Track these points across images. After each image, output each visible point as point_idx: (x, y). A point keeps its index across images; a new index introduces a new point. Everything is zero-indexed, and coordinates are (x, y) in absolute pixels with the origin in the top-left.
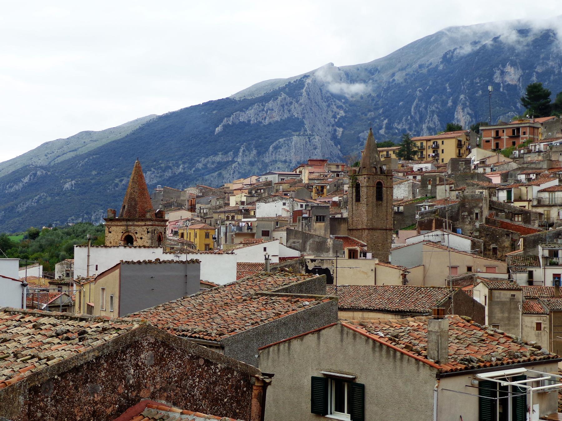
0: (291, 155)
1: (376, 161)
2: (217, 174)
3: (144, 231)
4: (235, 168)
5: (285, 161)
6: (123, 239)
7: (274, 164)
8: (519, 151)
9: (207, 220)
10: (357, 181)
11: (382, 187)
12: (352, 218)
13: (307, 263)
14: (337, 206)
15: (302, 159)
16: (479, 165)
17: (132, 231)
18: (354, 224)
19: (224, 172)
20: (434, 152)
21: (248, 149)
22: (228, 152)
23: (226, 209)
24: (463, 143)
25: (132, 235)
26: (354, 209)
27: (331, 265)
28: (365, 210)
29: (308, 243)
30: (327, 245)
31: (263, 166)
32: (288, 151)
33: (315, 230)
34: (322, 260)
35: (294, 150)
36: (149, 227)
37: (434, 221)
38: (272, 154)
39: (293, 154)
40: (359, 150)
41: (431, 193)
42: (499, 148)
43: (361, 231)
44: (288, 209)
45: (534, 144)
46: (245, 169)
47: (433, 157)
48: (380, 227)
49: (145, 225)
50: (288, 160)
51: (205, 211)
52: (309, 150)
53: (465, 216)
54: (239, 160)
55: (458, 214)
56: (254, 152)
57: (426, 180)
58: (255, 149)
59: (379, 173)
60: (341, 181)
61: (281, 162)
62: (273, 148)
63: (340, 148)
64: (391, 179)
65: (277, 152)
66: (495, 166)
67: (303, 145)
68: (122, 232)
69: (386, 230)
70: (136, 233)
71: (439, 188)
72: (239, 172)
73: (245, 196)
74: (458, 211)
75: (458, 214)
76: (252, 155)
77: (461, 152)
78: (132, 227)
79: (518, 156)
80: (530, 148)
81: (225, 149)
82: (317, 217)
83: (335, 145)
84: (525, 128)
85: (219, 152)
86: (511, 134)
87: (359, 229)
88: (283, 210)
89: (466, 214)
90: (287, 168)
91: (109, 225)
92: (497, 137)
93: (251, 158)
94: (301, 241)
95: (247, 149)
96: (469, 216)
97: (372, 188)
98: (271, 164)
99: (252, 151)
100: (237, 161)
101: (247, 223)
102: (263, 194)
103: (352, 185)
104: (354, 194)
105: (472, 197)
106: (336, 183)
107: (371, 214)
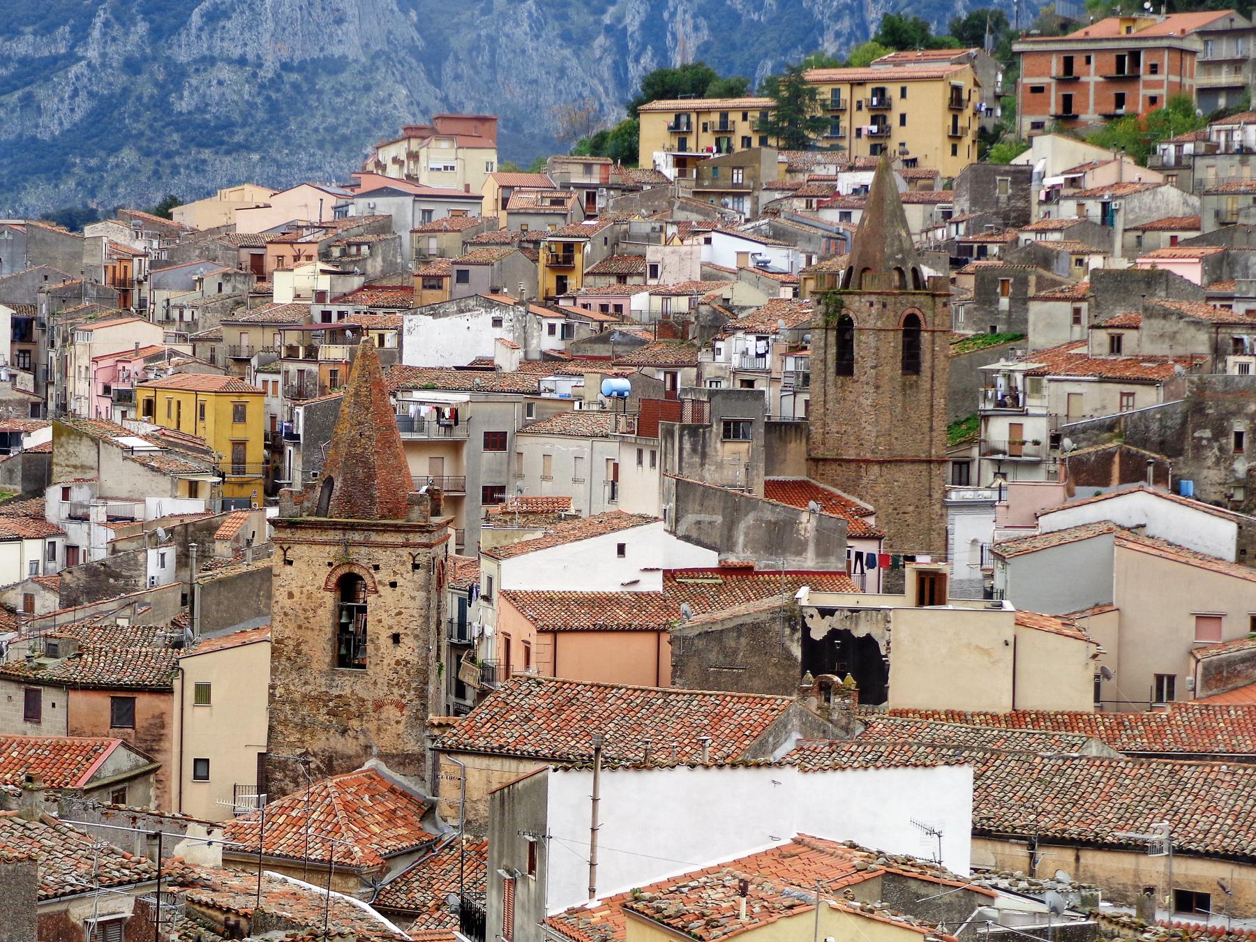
0: (263, 42)
1: (901, 250)
2: (20, 100)
3: (403, 563)
4: (77, 78)
5: (242, 61)
6: (331, 585)
7: (205, 70)
8: (1179, 146)
9: (199, 344)
10: (844, 312)
11: (919, 331)
12: (825, 425)
13: (808, 620)
14: (675, 335)
15: (298, 53)
17: (364, 562)
18: (830, 442)
19: (41, 93)
20: (874, 121)
21: (121, 17)
22: (56, 25)
23: (264, 313)
24: (965, 96)
25: (362, 572)
26: (830, 397)
28: (869, 402)
29: (742, 526)
30: (798, 530)
31: (170, 74)
32: (250, 28)
33: (720, 466)
34: (853, 611)
35: (270, 25)
36: (420, 550)
37: (1117, 459)
38: (199, 37)
39: (267, 36)
40: (477, 28)
42: (1074, 111)
43: (853, 466)
44: (509, 337)
45: (1229, 127)
46: (111, 84)
47: (871, 135)
48: (910, 454)
49: (405, 545)
50: (251, 57)
51: (187, 316)
52: (318, 25)
53: (1204, 442)
54: (93, 53)
55: (1181, 433)
56: (142, 28)
57: (995, 281)
58: (144, 19)
59: (911, 286)
60: (625, 227)
61: (230, 61)
62: (202, 16)
63: (415, 19)
64: (945, 305)
65: (215, 30)
66: (1114, 197)
67: (301, 8)
68: (330, 564)
69: (929, 462)
70: (377, 568)
71: (1035, 308)
72: (91, 95)
73: (324, 272)
74: (1184, 423)
75: (1181, 433)
76: (134, 38)
77: (960, 124)
78: (363, 550)
79: (1173, 161)
80: (1214, 138)
81: (42, 17)
83: (401, 10)
84: (1157, 55)
85: (25, 25)
86: (1112, 72)
88: (498, 344)
89: (1207, 433)
90: (247, 82)
91: (284, 541)
92: (1069, 76)
93: (129, 48)
94: (719, 519)
95: (117, 18)
96: (1217, 440)
97: (892, 333)
98: (197, 70)
99: (135, 25)
100: (83, 58)
101: (438, 410)
102: (369, 261)
103: (827, 322)
104: (833, 350)
105: (1226, 385)
106: (608, 234)
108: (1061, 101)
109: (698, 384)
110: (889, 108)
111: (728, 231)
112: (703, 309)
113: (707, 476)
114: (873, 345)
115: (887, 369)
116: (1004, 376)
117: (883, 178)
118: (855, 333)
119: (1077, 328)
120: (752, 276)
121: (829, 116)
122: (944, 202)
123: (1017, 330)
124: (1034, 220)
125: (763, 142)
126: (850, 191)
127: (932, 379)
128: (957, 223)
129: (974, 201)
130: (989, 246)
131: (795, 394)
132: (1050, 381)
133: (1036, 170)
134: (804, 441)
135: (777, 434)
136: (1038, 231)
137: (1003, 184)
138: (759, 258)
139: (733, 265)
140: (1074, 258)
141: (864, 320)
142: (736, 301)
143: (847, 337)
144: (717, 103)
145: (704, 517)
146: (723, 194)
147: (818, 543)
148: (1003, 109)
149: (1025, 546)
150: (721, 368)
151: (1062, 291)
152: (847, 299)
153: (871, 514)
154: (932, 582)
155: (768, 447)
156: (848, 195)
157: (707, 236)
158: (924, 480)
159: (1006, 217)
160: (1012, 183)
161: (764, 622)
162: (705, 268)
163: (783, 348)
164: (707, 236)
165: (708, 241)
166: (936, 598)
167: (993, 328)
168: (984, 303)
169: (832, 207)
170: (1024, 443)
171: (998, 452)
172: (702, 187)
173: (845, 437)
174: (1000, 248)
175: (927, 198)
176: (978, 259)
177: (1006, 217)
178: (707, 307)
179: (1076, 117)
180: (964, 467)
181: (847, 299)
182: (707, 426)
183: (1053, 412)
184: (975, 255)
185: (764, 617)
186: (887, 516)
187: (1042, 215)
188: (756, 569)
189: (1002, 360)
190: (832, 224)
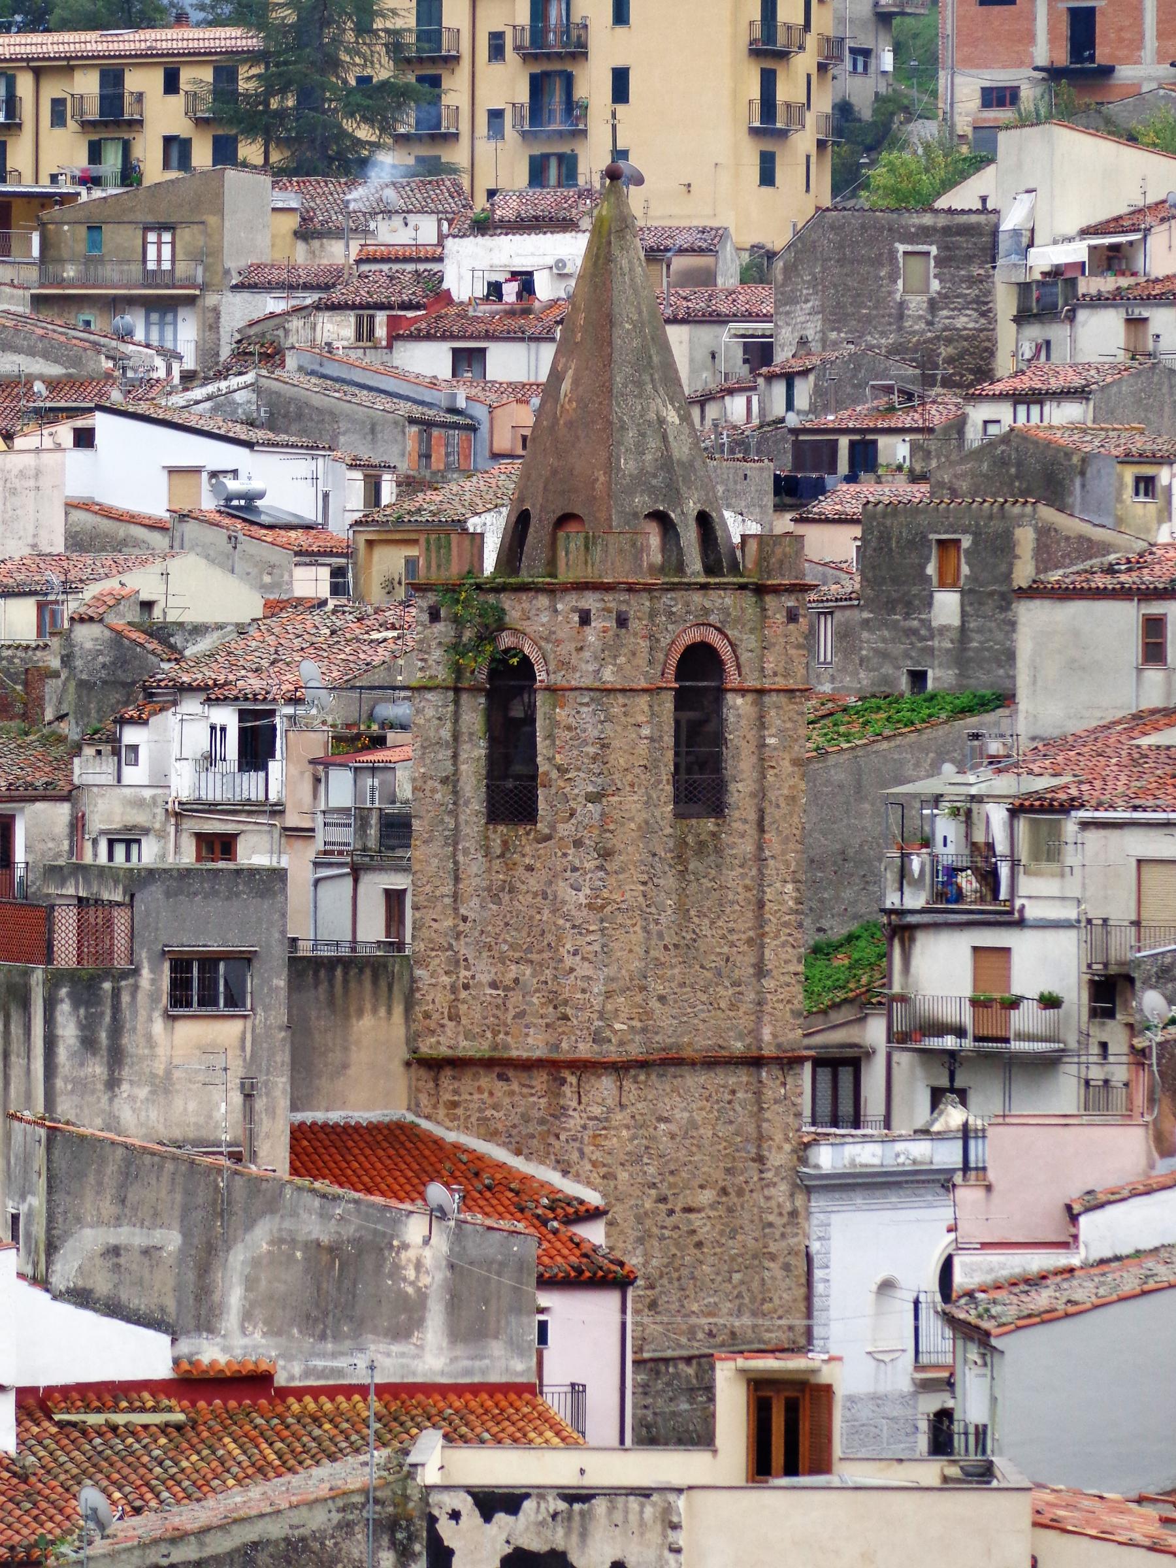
10: (506, 640)
11: (719, 693)
13: (445, 1528)
16: (1088, 285)
18: (472, 1013)
27: (654, 1536)
29: (238, 1259)
30: (397, 1267)
33: (163, 1086)
34: (575, 1496)
41: (961, 658)
42: (1103, 54)
43: (540, 1080)
48: (702, 1042)
57: (918, 543)
59: (694, 564)
69: (755, 1062)
82: (180, 965)
87: (528, 1066)
94: (171, 1240)
97: (643, 701)
103: (458, 670)
104: (475, 752)
107: (638, 935)
108: (1064, 28)
109: (75, 848)
110: (579, 52)
111: (142, 408)
112: (86, 635)
113: (127, 1116)
114: (593, 733)
115: (632, 804)
116: (955, 813)
117: (609, 259)
118: (540, 698)
119: (1154, 676)
120: (218, 537)
121: (411, 78)
122: (749, 317)
123: (983, 681)
124: (1004, 364)
125: (224, 153)
126: (481, 291)
127: (761, 829)
128: (789, 379)
129: (835, 317)
130: (883, 441)
131: (356, 872)
132: (1085, 825)
133: (1007, 225)
134: (398, 1010)
135: (323, 988)
136: (1018, 398)
137: (916, 264)
138: (232, 485)
139: (157, 507)
140: (1129, 474)
141: (564, 664)
142: (171, 611)
143: (517, 712)
144: (89, 42)
145: (131, 1236)
146: (116, 304)
147: (454, 1303)
148: (897, 51)
149: (1042, 1299)
150: (140, 803)
151: (1111, 570)
152: (514, 607)
153: (595, 1214)
154: (792, 1409)
155: (297, 1027)
156: (473, 301)
157: (80, 423)
158: (742, 1115)
159: (926, 361)
160: (940, 262)
161: (319, 1537)
162: (78, 516)
163: (316, 743)
164: (80, 423)
165: (85, 438)
166: (804, 1461)
167: (918, 678)
168: (890, 606)
169: (429, 337)
170: (1014, 1003)
171: (941, 1029)
172: (61, 283)
173: (515, 998)
174: (915, 448)
175: (698, 305)
176: (852, 478)
177: (926, 361)
178: (95, 630)
179: (1108, 71)
180: (846, 1075)
181: (514, 607)
182: (125, 974)
183: (1095, 913)
184: (843, 466)
185: (319, 1520)
186: (639, 1219)
187: (1027, 351)
188: (281, 1380)
189: (948, 768)
190: (433, 384)
